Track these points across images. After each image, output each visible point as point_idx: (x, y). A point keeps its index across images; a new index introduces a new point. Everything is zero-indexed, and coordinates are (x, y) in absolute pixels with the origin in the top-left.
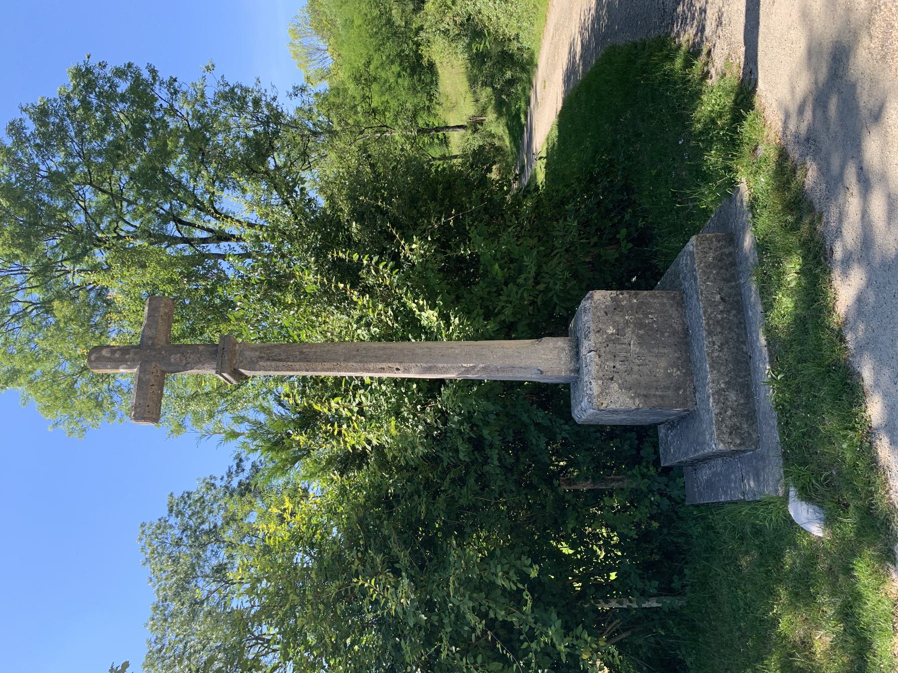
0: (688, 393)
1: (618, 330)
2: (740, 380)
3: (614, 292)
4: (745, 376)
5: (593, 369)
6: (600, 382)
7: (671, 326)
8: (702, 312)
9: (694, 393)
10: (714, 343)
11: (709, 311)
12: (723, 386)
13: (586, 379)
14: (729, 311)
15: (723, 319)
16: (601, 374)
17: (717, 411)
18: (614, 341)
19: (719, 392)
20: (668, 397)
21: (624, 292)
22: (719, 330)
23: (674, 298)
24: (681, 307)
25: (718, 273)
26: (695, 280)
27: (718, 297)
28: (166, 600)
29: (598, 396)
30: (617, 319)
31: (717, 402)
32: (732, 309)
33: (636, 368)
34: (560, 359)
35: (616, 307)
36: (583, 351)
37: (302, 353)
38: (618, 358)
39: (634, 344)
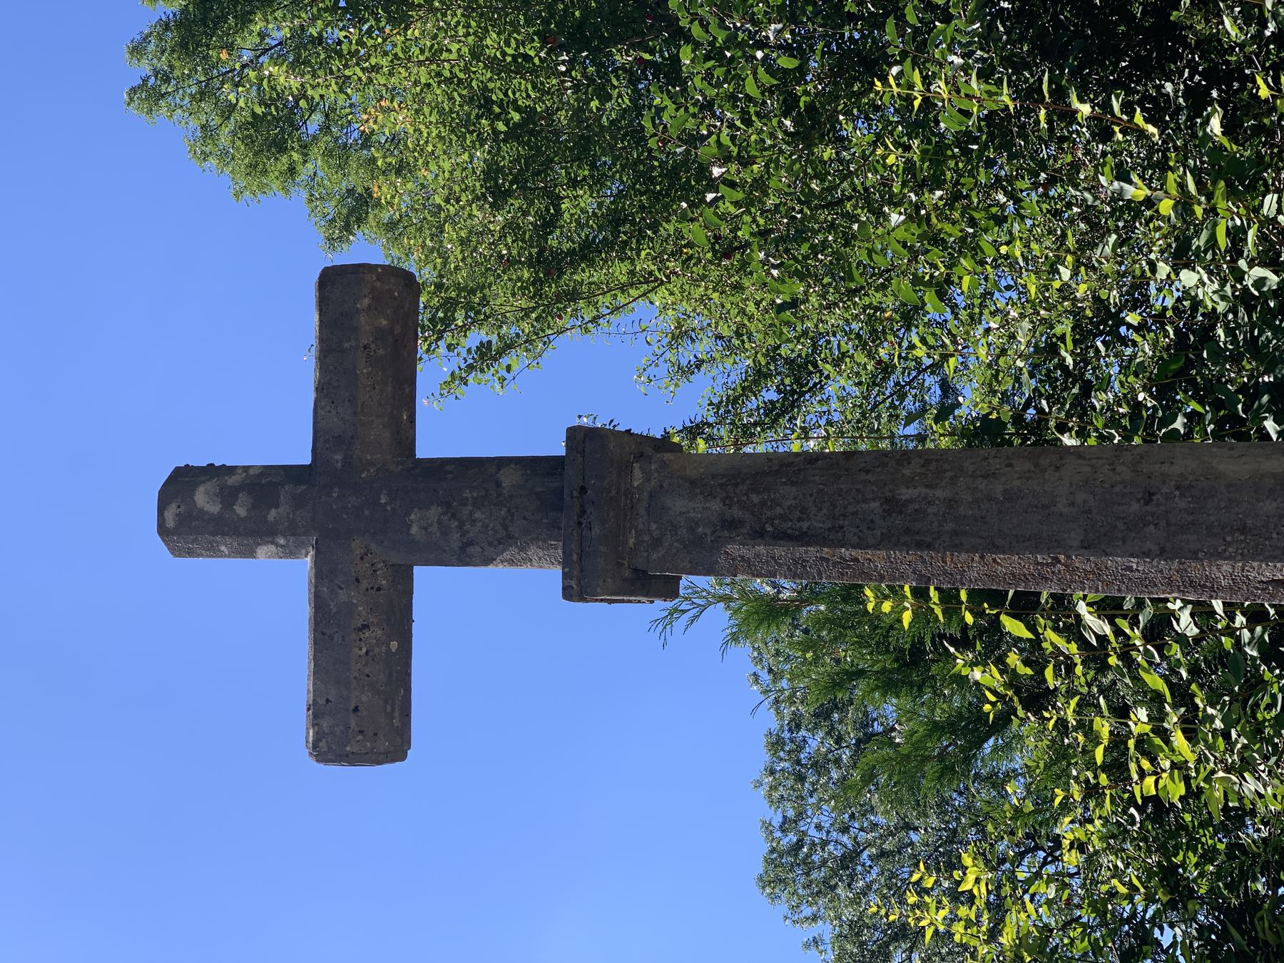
28: (798, 727)
37: (892, 505)
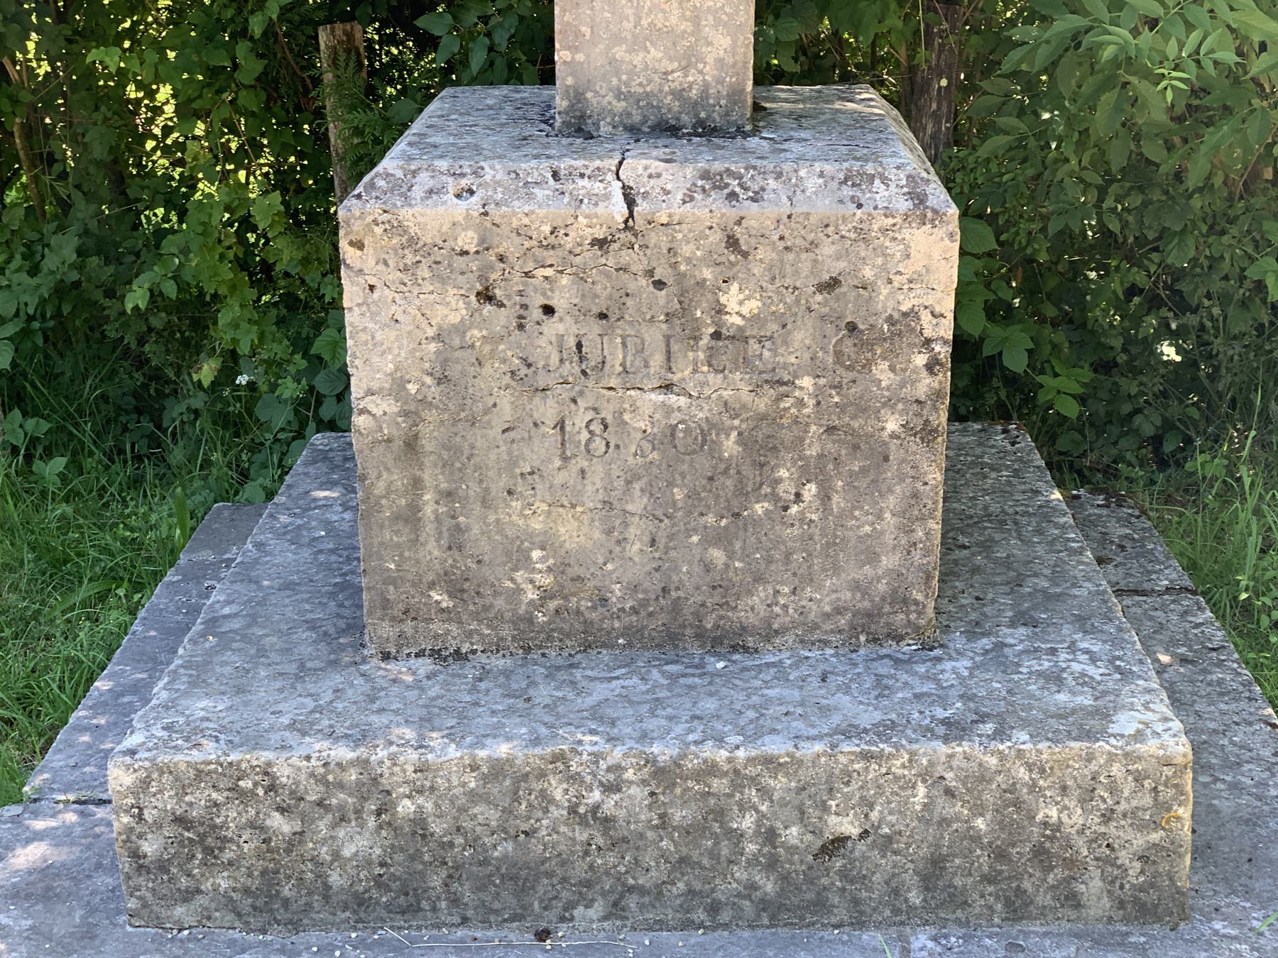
0: (438, 627)
1: (740, 337)
2: (436, 881)
3: (946, 329)
4: (455, 901)
5: (539, 209)
6: (467, 239)
7: (759, 579)
8: (776, 746)
9: (436, 654)
10: (609, 788)
11: (779, 784)
12: (406, 807)
13: (494, 171)
14: (772, 864)
15: (737, 837)
16: (510, 246)
17: (283, 773)
18: (679, 316)
19: (374, 792)
20: (415, 541)
21: (943, 379)
22: (678, 815)
23: (901, 600)
24: (854, 630)
25: (976, 839)
26: (955, 730)
27: (848, 826)
29: (397, 228)
30: (802, 336)
31: (327, 778)
32: (785, 878)
33: (547, 410)
34: (638, 44)
35: (860, 339)
36: (643, 165)
38: (593, 329)
39: (668, 410)
